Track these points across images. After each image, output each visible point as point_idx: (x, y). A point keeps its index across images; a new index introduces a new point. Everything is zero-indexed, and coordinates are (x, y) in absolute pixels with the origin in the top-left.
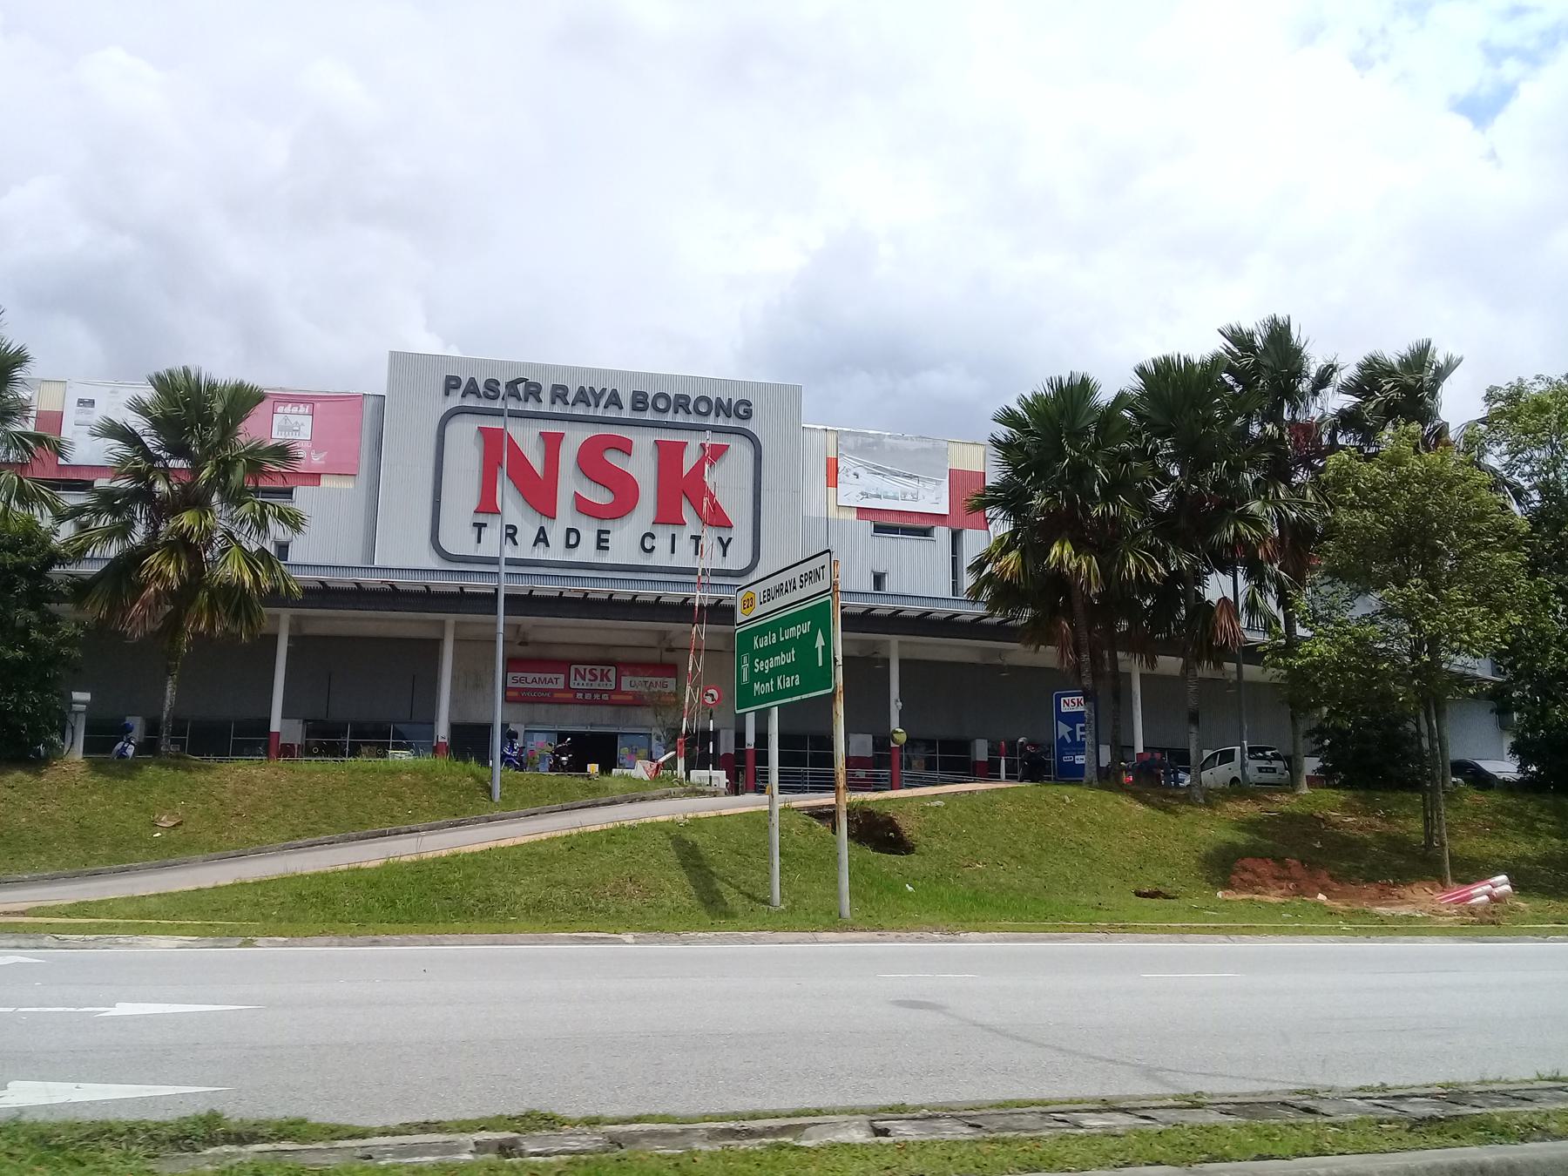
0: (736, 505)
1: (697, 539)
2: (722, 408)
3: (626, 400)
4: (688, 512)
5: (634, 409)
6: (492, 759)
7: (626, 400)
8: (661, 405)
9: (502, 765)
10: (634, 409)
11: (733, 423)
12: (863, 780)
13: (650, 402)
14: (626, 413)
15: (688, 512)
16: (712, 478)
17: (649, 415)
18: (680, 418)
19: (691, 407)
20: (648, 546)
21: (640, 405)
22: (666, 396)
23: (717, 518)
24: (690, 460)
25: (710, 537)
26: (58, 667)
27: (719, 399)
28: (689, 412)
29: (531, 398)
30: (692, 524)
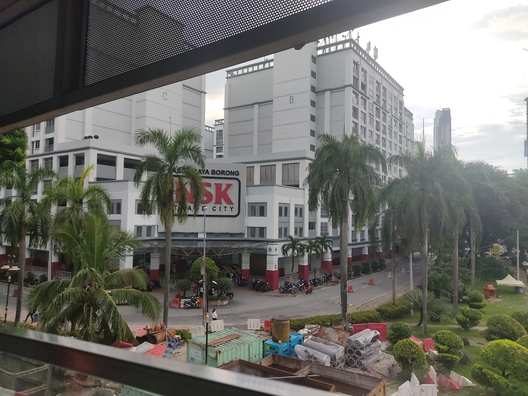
0: (234, 198)
1: (225, 207)
2: (232, 173)
3: (210, 172)
4: (223, 201)
5: (212, 174)
6: (501, 317)
7: (210, 172)
8: (218, 173)
9: (422, 306)
10: (212, 174)
11: (235, 176)
12: (290, 276)
13: (215, 172)
14: (211, 175)
15: (223, 201)
16: (229, 193)
17: (216, 176)
18: (223, 176)
19: (225, 173)
20: (214, 210)
21: (213, 173)
22: (229, 171)
23: (229, 202)
24: (223, 188)
25: (229, 206)
26: (29, 224)
27: (231, 171)
28: (234, 175)
29: (223, 174)
30: (224, 204)
